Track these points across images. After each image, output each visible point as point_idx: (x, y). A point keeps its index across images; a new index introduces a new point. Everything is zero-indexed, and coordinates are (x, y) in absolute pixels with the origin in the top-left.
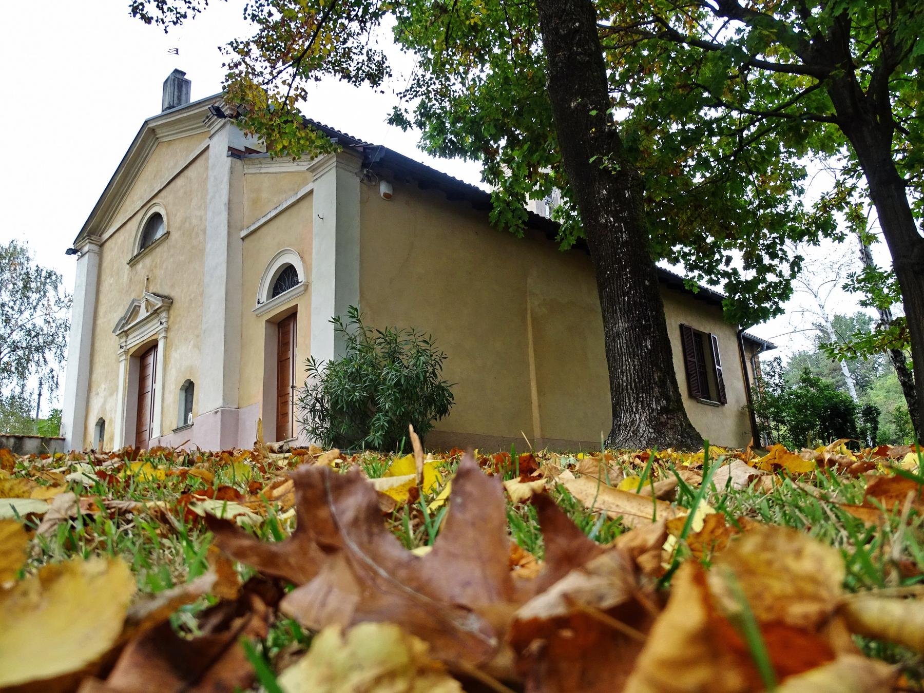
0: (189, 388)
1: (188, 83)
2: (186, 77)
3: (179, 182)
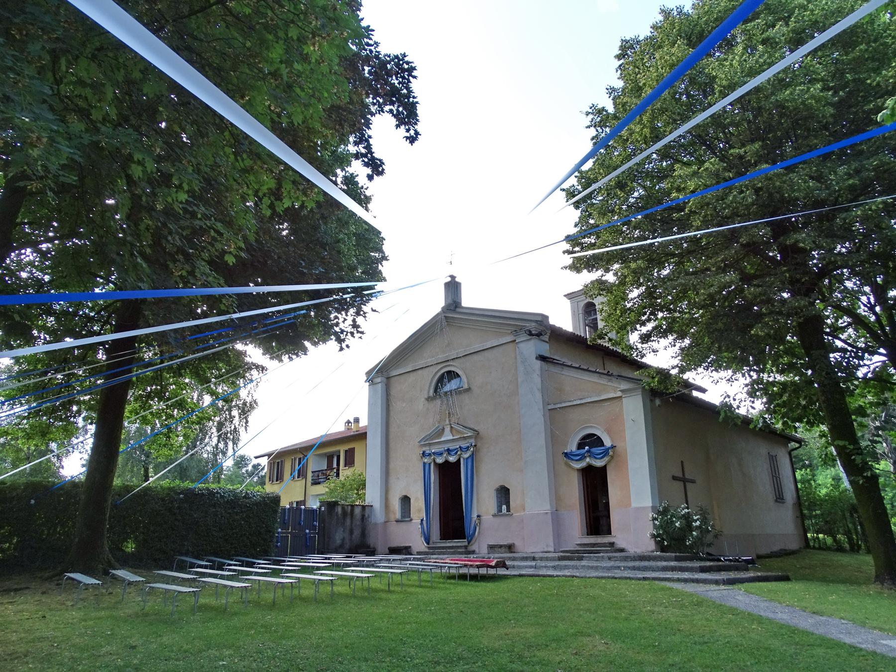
0: (504, 494)
3: (475, 357)
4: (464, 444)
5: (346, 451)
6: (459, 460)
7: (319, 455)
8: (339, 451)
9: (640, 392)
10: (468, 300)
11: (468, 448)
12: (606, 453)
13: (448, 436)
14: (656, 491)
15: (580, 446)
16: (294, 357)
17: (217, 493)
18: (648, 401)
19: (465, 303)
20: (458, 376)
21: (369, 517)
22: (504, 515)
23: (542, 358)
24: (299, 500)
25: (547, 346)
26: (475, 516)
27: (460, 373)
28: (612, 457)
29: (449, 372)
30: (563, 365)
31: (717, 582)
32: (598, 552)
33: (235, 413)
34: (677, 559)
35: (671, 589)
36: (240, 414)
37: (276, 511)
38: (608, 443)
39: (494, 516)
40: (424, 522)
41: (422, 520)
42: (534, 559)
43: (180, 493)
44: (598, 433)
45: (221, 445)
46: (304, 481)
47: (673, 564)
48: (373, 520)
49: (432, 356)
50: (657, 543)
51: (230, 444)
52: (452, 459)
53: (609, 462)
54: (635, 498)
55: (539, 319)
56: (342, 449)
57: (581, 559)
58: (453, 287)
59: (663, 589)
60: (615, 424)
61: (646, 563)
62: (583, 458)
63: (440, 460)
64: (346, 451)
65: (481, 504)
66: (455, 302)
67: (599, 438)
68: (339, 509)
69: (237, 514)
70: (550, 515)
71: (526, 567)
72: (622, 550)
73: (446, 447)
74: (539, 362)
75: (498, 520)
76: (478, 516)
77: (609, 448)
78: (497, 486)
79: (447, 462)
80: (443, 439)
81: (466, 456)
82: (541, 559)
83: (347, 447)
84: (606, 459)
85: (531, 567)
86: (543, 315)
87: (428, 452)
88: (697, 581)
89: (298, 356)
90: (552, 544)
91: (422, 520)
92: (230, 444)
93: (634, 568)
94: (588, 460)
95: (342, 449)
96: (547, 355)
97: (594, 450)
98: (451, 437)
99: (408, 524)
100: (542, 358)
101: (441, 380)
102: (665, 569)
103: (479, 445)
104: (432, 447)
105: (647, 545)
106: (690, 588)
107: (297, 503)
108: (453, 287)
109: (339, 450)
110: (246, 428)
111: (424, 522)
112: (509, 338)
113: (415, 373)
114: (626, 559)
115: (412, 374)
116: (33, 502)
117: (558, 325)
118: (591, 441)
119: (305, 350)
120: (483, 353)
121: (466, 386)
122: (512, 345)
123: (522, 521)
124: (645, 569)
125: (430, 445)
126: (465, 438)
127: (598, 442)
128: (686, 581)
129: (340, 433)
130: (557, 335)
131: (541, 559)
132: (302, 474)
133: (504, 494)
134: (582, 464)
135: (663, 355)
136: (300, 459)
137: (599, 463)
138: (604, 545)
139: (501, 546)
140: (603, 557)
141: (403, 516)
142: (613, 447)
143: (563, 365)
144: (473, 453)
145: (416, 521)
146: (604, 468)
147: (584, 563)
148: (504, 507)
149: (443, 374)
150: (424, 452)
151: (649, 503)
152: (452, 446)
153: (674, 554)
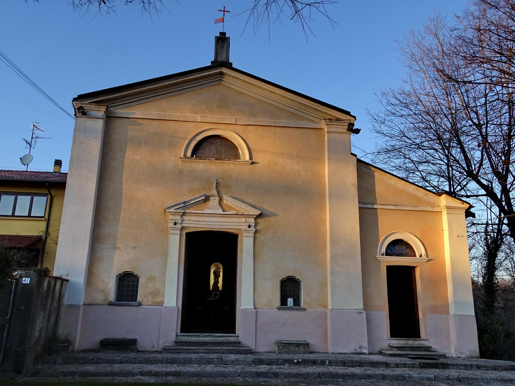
22: (290, 309)
80: (206, 211)
108: (222, 40)
148: (290, 301)
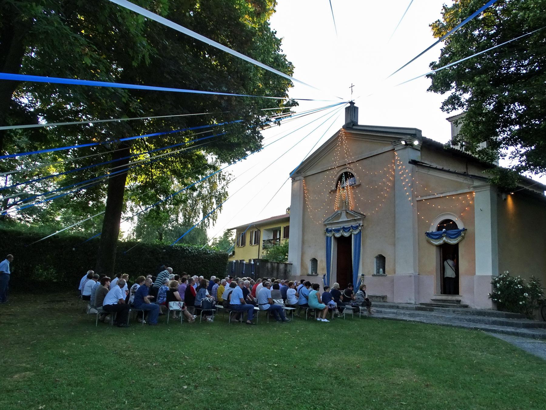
0: (381, 260)
1: (357, 108)
2: (355, 105)
4: (354, 224)
5: (285, 228)
6: (351, 236)
7: (268, 230)
8: (280, 228)
9: (488, 188)
10: (363, 120)
11: (357, 227)
12: (459, 233)
13: (344, 218)
14: (497, 264)
15: (439, 228)
16: (237, 160)
17: (187, 249)
18: (495, 195)
19: (360, 123)
20: (352, 176)
21: (290, 271)
22: (382, 276)
23: (414, 162)
24: (255, 258)
25: (419, 154)
26: (360, 275)
27: (355, 174)
28: (463, 237)
29: (346, 173)
30: (430, 168)
31: (533, 337)
32: (447, 306)
33: (214, 200)
34: (508, 316)
35: (493, 338)
36: (217, 201)
37: (225, 264)
38: (460, 226)
39: (374, 275)
40: (326, 277)
41: (324, 276)
42: (398, 307)
43: (164, 248)
44: (455, 219)
45: (206, 221)
46: (258, 246)
47: (501, 319)
48: (292, 273)
49: (335, 160)
50: (494, 302)
51: (211, 220)
52: (346, 235)
53: (461, 241)
54: (481, 267)
55: (413, 132)
56: (282, 226)
57: (432, 310)
58: (352, 110)
59: (488, 337)
60: (469, 215)
61: (486, 318)
62: (440, 237)
63: (338, 235)
64: (285, 228)
65: (365, 268)
66: (352, 122)
67: (454, 223)
68: (269, 265)
69: (200, 263)
70: (413, 278)
71: (390, 313)
72: (466, 306)
73: (342, 225)
74: (411, 165)
75: (376, 278)
76: (363, 275)
77: (461, 231)
78: (377, 255)
79: (342, 236)
80: (340, 220)
81: (356, 232)
82: (403, 308)
83: (285, 225)
84: (459, 238)
85: (394, 313)
86: (416, 129)
87: (330, 229)
88: (517, 334)
89: (239, 160)
90: (413, 298)
91: (324, 276)
92: (211, 220)
93: (470, 320)
94: (444, 238)
95: (282, 226)
96: (418, 159)
97: (450, 232)
98: (346, 219)
99: (315, 277)
100: (414, 162)
101: (340, 179)
102: (494, 323)
103: (365, 225)
104: (333, 226)
105: (487, 304)
106: (508, 339)
107: (254, 260)
108: (352, 110)
109: (277, 226)
110: (220, 210)
111: (326, 277)
112: (390, 148)
113: (323, 173)
114: (466, 313)
115: (321, 174)
116: (74, 249)
117: (428, 137)
118: (448, 226)
119: (244, 156)
120: (370, 158)
121: (357, 183)
122: (392, 152)
123: (393, 280)
124: (480, 321)
125: (331, 224)
126: (355, 220)
127: (455, 226)
128: (502, 332)
129: (283, 216)
130: (429, 146)
131: (403, 308)
132: (257, 242)
133: (381, 260)
134: (441, 242)
135: (509, 158)
136: (256, 232)
137: (453, 242)
138: (452, 301)
139: (377, 297)
140: (449, 310)
141: (312, 272)
142: (464, 230)
143: (430, 168)
144: (360, 231)
145: (321, 276)
146: (457, 245)
147: (433, 313)
148: (381, 270)
149: (342, 174)
150: (327, 229)
151: (490, 273)
152: (347, 225)
153: (505, 313)
